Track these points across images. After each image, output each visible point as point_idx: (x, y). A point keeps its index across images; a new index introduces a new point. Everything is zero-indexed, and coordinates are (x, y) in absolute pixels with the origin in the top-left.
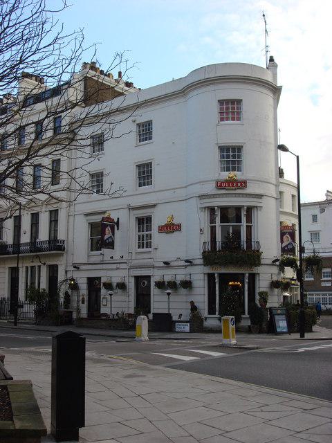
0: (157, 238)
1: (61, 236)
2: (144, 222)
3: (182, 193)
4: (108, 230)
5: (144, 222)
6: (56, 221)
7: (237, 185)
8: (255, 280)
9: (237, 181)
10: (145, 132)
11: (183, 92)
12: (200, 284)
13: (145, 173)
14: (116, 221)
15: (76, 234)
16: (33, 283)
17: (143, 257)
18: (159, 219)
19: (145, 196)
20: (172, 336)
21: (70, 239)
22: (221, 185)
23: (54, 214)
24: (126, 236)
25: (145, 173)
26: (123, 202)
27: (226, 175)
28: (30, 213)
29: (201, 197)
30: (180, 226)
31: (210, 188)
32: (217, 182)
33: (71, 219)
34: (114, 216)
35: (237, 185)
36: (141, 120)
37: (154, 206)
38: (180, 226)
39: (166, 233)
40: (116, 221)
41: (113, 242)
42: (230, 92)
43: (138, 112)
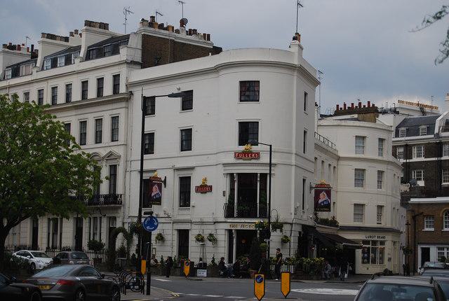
0: (195, 197)
1: (119, 191)
2: (185, 183)
3: (212, 160)
4: (155, 189)
5: (185, 183)
6: (231, 189)
7: (251, 156)
8: (299, 247)
9: (251, 153)
10: (187, 100)
11: (216, 69)
12: (222, 238)
13: (186, 139)
14: (163, 179)
15: (130, 189)
16: (95, 228)
17: (185, 214)
18: (195, 182)
19: (186, 160)
20: (196, 278)
21: (127, 194)
22: (238, 156)
23: (113, 169)
24: (171, 193)
25: (186, 139)
26: (170, 163)
27: (242, 148)
28: (108, 165)
29: (225, 165)
30: (211, 187)
31: (231, 159)
32: (235, 153)
33: (128, 173)
34: (161, 175)
35: (251, 156)
36: (148, 95)
37: (192, 168)
38: (211, 187)
39: (202, 193)
40: (163, 179)
41: (160, 198)
42: (249, 75)
43: (145, 87)
